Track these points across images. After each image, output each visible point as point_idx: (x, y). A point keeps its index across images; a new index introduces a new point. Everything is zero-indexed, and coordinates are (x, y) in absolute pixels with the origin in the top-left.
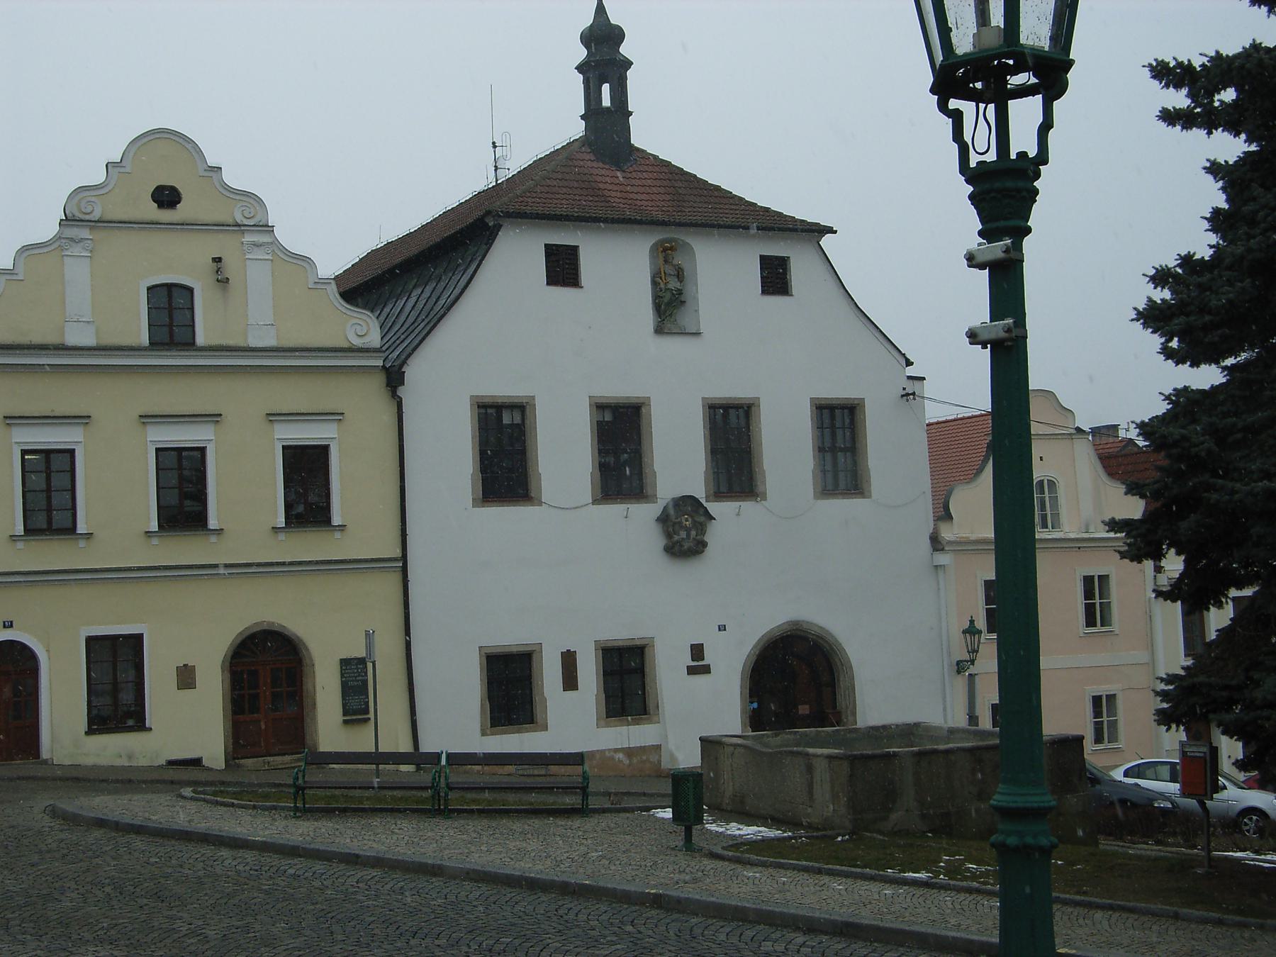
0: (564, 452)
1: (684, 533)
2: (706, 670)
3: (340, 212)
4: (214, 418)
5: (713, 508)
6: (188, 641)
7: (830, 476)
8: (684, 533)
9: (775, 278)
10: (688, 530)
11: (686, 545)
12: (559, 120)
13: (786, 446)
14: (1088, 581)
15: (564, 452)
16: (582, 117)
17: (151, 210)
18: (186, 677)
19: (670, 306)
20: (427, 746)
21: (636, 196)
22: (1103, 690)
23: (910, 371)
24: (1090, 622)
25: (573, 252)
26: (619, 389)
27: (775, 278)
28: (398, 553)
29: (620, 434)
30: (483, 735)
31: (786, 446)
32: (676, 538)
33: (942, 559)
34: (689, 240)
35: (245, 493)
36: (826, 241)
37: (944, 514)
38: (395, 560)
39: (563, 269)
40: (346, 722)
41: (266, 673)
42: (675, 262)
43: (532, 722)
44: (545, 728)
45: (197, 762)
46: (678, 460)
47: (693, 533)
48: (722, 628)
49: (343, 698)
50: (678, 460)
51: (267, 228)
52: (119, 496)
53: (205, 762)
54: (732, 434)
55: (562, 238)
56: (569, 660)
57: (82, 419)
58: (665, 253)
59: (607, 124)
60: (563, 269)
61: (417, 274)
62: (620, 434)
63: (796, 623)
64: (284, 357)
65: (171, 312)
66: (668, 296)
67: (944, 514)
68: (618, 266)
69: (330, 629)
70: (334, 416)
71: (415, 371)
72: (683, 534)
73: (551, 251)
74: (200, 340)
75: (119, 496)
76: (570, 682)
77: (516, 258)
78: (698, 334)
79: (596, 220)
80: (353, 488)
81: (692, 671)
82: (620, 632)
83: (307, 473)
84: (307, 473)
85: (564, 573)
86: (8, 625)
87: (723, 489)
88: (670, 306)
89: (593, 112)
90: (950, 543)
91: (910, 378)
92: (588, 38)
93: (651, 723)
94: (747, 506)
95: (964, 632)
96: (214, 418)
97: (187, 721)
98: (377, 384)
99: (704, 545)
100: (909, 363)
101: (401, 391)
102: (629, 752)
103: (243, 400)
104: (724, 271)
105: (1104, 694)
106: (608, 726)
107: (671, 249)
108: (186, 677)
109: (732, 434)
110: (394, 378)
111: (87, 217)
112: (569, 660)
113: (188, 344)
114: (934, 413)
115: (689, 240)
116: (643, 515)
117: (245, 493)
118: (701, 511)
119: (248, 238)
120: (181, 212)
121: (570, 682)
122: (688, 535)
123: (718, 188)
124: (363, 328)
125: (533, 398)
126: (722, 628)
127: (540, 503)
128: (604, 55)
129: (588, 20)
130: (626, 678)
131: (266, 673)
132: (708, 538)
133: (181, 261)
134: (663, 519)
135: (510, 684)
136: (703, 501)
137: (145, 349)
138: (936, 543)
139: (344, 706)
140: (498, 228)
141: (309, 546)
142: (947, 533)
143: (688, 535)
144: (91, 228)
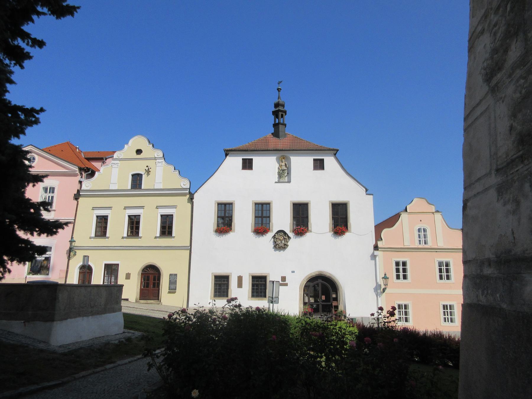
0: (244, 218)
4: (110, 208)
11: (280, 245)
14: (440, 264)
15: (244, 218)
17: (135, 156)
19: (284, 174)
25: (251, 161)
26: (339, 199)
28: (189, 245)
29: (262, 213)
31: (320, 218)
33: (376, 253)
34: (288, 155)
35: (150, 226)
39: (247, 165)
47: (283, 242)
50: (282, 219)
52: (118, 227)
53: (129, 300)
54: (301, 214)
56: (240, 279)
57: (110, 208)
62: (262, 213)
65: (137, 180)
70: (175, 207)
72: (280, 242)
75: (118, 227)
76: (240, 285)
79: (247, 151)
87: (99, 234)
88: (284, 174)
95: (383, 278)
99: (287, 246)
103: (150, 202)
106: (252, 300)
109: (301, 214)
112: (240, 279)
115: (288, 155)
117: (150, 226)
119: (157, 161)
120: (142, 156)
121: (240, 285)
122: (281, 242)
132: (289, 244)
134: (274, 237)
135: (221, 285)
138: (376, 248)
142: (380, 244)
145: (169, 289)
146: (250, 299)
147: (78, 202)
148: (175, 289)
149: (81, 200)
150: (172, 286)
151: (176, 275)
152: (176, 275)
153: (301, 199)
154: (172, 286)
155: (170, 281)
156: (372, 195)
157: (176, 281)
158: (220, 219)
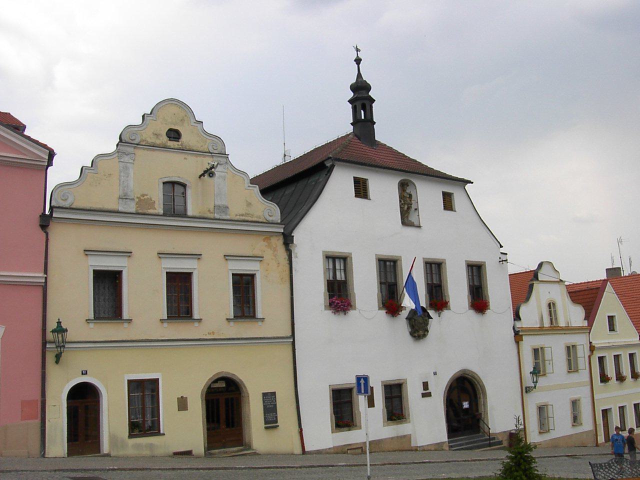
0: (365, 285)
2: (429, 395)
3: (258, 152)
4: (198, 256)
5: (431, 313)
6: (183, 384)
7: (383, 274)
8: (418, 326)
9: (448, 203)
12: (340, 123)
15: (365, 285)
16: (352, 124)
17: (164, 139)
18: (183, 404)
19: (407, 210)
21: (392, 156)
23: (502, 250)
27: (448, 203)
28: (290, 334)
30: (332, 433)
35: (212, 298)
36: (468, 187)
37: (517, 317)
38: (287, 338)
39: (361, 189)
40: (266, 428)
41: (224, 405)
42: (408, 191)
45: (189, 453)
48: (435, 374)
49: (265, 415)
51: (226, 156)
52: (144, 296)
53: (194, 453)
58: (403, 186)
59: (364, 123)
60: (361, 189)
61: (294, 186)
63: (465, 370)
64: (247, 225)
67: (517, 317)
69: (257, 378)
71: (299, 235)
74: (190, 213)
75: (144, 296)
77: (340, 181)
78: (419, 227)
80: (266, 296)
81: (424, 395)
83: (244, 286)
84: (244, 286)
85: (367, 345)
86: (85, 373)
89: (356, 122)
91: (502, 253)
92: (354, 88)
93: (407, 423)
96: (198, 256)
97: (184, 428)
98: (279, 242)
100: (501, 247)
101: (291, 247)
104: (427, 196)
106: (388, 425)
108: (183, 404)
110: (288, 240)
111: (132, 142)
113: (184, 215)
114: (513, 269)
117: (212, 298)
118: (426, 314)
124: (270, 210)
130: (395, 402)
131: (224, 405)
133: (184, 168)
137: (161, 216)
139: (265, 418)
140: (333, 166)
141: (246, 329)
144: (135, 148)
145: (266, 423)
146: (408, 420)
147: (47, 234)
148: (276, 422)
149: (57, 232)
150: (270, 418)
151: (274, 394)
152: (274, 394)
153: (435, 255)
154: (270, 416)
155: (265, 407)
156: (92, 166)
157: (275, 406)
158: (383, 286)
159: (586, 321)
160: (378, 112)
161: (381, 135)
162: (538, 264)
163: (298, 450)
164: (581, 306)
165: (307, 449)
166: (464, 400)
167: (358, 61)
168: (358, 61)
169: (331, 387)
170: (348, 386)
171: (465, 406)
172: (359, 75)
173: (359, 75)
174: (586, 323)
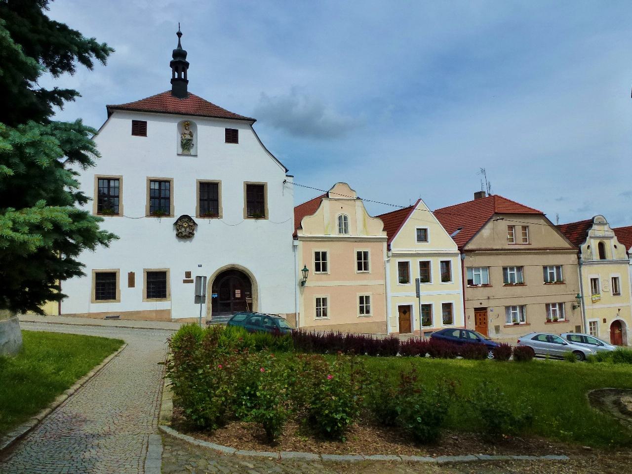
1: (185, 229)
5: (198, 221)
8: (185, 229)
10: (185, 228)
11: (184, 234)
13: (233, 200)
19: (187, 145)
20: (467, 328)
22: (364, 294)
24: (360, 268)
27: (232, 137)
31: (233, 200)
32: (180, 231)
33: (296, 243)
37: (298, 226)
43: (114, 298)
44: (119, 301)
46: (185, 201)
48: (200, 266)
50: (185, 201)
55: (140, 118)
56: (131, 277)
59: (179, 85)
60: (139, 129)
66: (185, 141)
67: (298, 226)
68: (164, 131)
72: (183, 229)
73: (135, 123)
76: (131, 283)
81: (185, 281)
82: (155, 267)
88: (187, 145)
90: (300, 237)
94: (214, 221)
102: (156, 311)
105: (364, 296)
107: (188, 125)
112: (131, 277)
115: (194, 121)
116: (167, 224)
121: (131, 283)
122: (185, 230)
123: (218, 107)
125: (122, 176)
126: (200, 266)
127: (123, 216)
128: (179, 62)
129: (176, 47)
130: (157, 284)
136: (194, 219)
138: (295, 237)
142: (300, 234)
143: (185, 230)
159: (385, 233)
160: (191, 74)
161: (191, 89)
162: (610, 325)
163: (57, 314)
164: (73, 123)
165: (62, 313)
166: (232, 288)
167: (179, 34)
168: (179, 34)
169: (94, 271)
170: (112, 271)
171: (485, 234)
172: (179, 45)
173: (179, 45)
174: (384, 235)
